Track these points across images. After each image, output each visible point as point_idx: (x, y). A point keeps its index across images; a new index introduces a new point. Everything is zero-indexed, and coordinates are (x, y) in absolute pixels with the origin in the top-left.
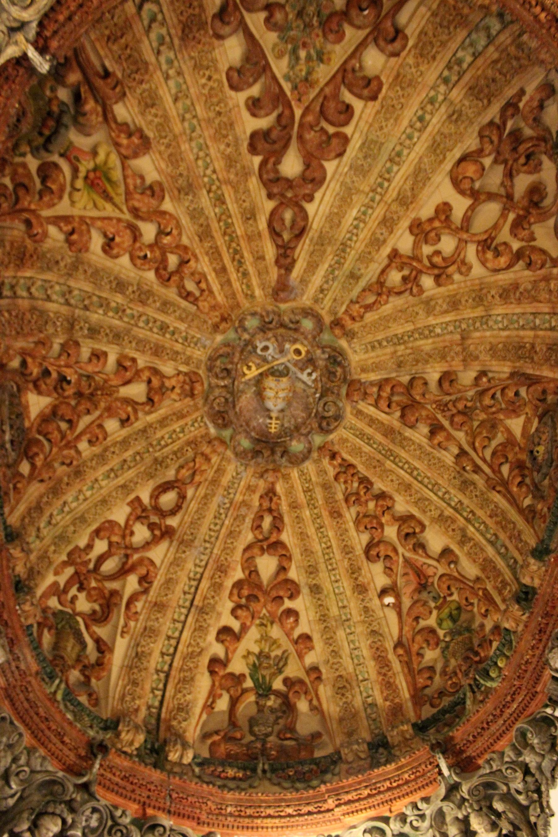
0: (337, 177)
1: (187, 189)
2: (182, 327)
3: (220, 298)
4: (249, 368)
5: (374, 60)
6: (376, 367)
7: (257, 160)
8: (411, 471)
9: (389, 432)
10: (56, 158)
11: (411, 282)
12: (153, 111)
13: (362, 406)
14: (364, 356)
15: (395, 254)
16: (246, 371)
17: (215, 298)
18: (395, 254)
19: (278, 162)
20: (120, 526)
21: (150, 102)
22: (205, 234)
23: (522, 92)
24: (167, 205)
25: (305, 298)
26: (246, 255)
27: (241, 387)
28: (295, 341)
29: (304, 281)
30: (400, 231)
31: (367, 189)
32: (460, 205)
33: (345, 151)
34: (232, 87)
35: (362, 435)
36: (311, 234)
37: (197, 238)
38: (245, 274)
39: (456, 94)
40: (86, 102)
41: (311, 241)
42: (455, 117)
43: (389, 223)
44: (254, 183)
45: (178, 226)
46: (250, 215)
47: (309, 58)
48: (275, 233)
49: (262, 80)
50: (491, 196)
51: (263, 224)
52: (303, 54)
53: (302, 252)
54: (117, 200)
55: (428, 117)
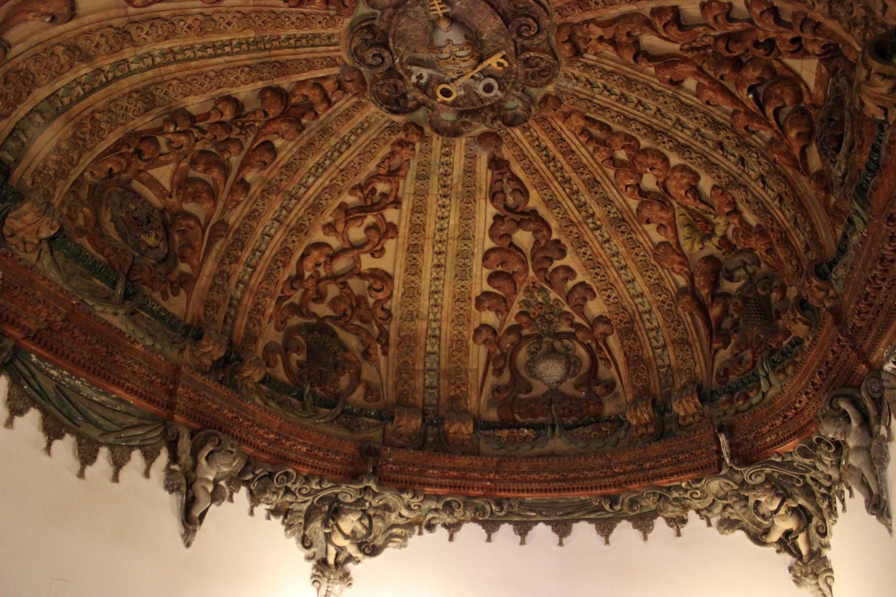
0: (481, 241)
3: (559, 124)
4: (499, 64)
5: (489, 317)
6: (347, 115)
7: (555, 236)
8: (217, 50)
9: (283, 68)
12: (652, 280)
15: (397, 203)
16: (502, 61)
18: (397, 203)
19: (537, 242)
21: (657, 287)
22: (593, 184)
23: (385, 353)
27: (503, 40)
28: (454, 104)
29: (471, 158)
31: (450, 241)
33: (483, 261)
35: (310, 41)
36: (484, 194)
37: (599, 179)
39: (423, 325)
40: (707, 294)
41: (481, 189)
42: (415, 313)
43: (417, 228)
46: (551, 203)
53: (484, 174)
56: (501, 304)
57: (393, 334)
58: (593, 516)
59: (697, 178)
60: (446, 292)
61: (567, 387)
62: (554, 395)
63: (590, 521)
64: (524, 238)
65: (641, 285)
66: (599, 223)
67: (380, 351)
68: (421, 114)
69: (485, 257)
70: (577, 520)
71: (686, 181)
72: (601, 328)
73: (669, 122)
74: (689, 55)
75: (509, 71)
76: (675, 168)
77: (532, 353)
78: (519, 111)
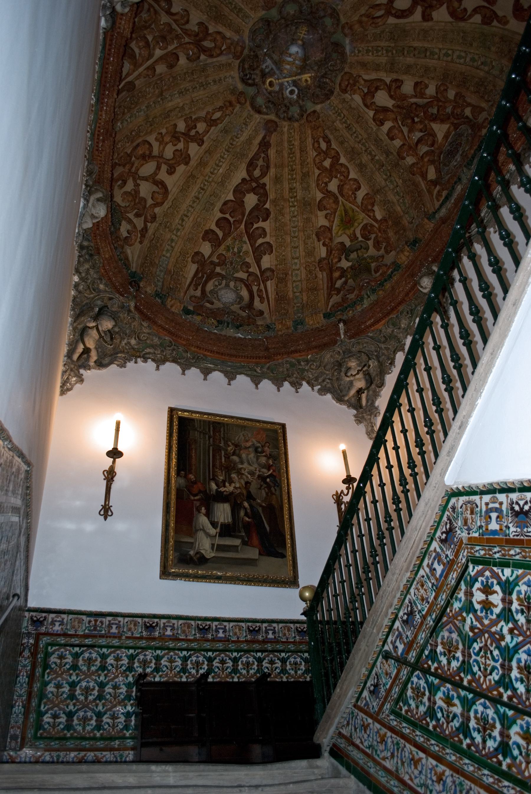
1: (306, 204)
2: (338, 124)
7: (267, 206)
10: (360, 239)
11: (190, 126)
13: (236, 38)
14: (227, 74)
16: (309, 79)
17: (312, 134)
18: (201, 143)
20: (448, 8)
21: (310, 253)
24: (319, 196)
25: (258, 120)
26: (286, 155)
28: (270, 93)
30: (196, 158)
31: (213, 184)
32: (163, 175)
33: (223, 205)
34: (271, 246)
38: (289, 142)
43: (202, 164)
44: (272, 196)
45: (318, 185)
46: (277, 180)
47: (233, 248)
48: (267, 160)
49: (257, 245)
50: (145, 179)
51: (272, 171)
52: (236, 250)
54: (343, 208)
55: (180, 222)
56: (216, 243)
57: (150, 232)
58: (249, 373)
59: (359, 188)
60: (191, 219)
61: (235, 308)
62: (226, 310)
63: (247, 375)
64: (251, 200)
65: (301, 251)
66: (295, 204)
67: (139, 240)
68: (251, 91)
69: (225, 203)
70: (240, 373)
71: (355, 186)
72: (268, 274)
73: (364, 149)
74: (395, 110)
75: (308, 87)
76: (351, 179)
77: (216, 286)
78: (296, 115)
